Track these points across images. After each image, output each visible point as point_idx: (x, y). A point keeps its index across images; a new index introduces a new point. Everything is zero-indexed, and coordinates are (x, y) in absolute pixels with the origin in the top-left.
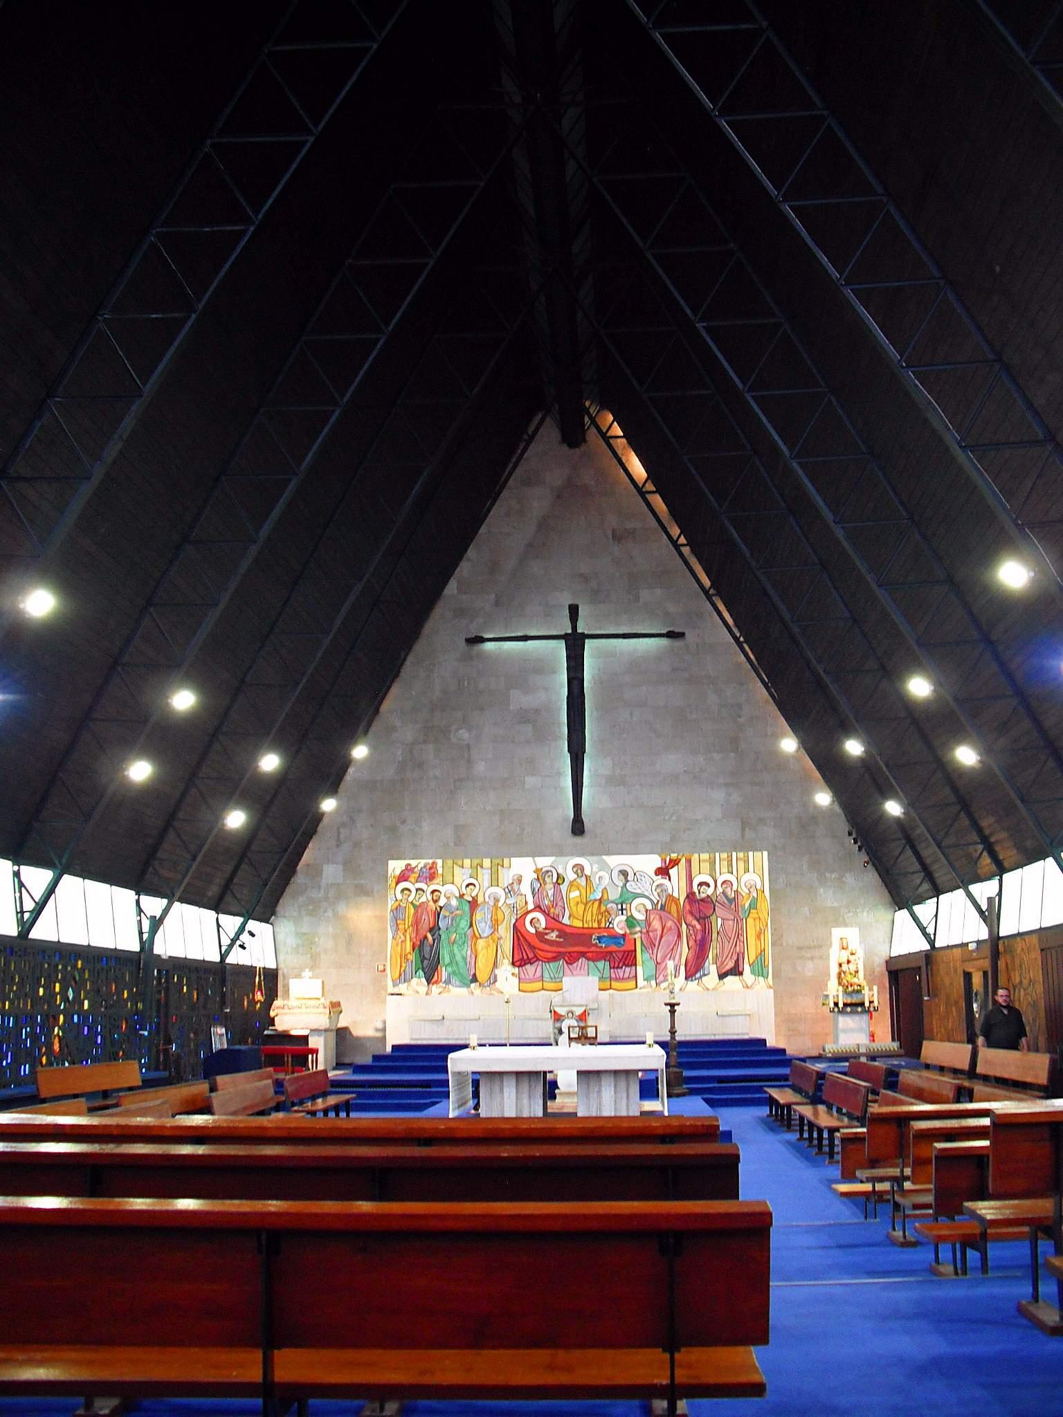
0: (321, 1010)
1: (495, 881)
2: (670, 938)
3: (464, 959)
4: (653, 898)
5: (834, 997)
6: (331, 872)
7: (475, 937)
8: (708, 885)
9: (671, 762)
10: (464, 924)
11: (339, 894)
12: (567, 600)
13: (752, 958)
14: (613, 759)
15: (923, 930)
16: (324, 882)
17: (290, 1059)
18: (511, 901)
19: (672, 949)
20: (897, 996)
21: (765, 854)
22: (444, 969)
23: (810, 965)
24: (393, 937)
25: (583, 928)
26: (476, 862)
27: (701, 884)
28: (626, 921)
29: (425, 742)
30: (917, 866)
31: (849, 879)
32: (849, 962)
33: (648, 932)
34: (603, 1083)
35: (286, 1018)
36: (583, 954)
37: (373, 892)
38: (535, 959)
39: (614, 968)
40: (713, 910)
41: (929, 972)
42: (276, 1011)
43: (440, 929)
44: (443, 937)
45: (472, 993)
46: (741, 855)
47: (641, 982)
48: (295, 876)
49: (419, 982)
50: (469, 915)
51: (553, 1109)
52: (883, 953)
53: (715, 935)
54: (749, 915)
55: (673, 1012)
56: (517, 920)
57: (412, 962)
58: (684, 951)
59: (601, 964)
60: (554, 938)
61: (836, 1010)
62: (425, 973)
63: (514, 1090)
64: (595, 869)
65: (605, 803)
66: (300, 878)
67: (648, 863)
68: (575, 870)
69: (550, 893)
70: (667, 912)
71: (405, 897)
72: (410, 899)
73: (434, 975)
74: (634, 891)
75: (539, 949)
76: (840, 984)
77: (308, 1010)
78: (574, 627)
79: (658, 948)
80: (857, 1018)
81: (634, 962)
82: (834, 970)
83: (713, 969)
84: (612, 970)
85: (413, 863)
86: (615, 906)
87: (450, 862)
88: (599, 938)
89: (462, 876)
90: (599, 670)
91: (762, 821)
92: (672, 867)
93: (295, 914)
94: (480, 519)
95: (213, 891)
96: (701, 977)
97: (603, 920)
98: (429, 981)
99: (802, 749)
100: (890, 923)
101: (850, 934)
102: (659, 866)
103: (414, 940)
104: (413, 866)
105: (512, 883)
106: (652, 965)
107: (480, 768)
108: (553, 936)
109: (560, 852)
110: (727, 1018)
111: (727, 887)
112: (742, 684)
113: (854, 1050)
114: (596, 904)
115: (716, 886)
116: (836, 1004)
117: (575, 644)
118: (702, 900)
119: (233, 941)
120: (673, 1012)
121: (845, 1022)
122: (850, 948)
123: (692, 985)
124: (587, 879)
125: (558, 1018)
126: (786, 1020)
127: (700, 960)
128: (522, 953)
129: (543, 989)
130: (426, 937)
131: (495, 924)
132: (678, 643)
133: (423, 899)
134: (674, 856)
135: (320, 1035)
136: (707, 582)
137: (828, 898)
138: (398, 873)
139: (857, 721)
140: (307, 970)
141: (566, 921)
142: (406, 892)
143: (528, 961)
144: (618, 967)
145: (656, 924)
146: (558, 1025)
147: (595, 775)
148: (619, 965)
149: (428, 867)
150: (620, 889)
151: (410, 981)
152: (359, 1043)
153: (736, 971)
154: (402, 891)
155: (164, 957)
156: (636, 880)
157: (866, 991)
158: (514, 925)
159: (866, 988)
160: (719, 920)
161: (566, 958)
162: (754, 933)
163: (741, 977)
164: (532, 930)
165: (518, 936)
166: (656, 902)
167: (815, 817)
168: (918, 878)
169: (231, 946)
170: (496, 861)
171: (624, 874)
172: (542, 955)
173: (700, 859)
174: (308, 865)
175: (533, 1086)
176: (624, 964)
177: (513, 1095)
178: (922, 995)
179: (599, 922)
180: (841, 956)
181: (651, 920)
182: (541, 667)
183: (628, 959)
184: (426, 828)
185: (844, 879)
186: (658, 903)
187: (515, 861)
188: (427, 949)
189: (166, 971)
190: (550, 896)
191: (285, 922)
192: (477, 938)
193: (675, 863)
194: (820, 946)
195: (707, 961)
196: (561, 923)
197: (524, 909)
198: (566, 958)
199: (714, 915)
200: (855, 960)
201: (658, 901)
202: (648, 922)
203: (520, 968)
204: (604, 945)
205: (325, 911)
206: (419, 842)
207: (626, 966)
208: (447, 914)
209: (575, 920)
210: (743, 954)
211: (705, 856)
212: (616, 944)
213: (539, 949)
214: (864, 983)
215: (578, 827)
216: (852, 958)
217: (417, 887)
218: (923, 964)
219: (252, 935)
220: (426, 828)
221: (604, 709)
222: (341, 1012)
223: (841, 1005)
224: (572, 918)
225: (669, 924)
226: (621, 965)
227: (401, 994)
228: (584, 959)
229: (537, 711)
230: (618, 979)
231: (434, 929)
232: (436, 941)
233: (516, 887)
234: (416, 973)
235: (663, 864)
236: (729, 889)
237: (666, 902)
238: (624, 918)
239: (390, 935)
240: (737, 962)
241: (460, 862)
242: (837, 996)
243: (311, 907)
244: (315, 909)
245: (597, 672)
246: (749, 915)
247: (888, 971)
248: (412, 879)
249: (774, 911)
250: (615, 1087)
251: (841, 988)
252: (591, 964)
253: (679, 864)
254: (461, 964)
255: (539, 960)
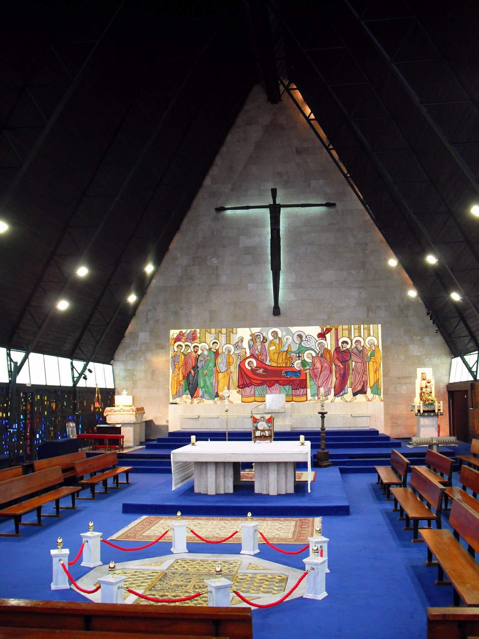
0: (131, 412)
1: (228, 341)
2: (326, 372)
3: (212, 384)
4: (316, 350)
5: (418, 407)
6: (143, 336)
7: (218, 372)
8: (347, 343)
9: (329, 275)
10: (211, 364)
11: (148, 348)
12: (270, 186)
13: (372, 384)
14: (296, 274)
15: (470, 369)
16: (139, 343)
17: (107, 441)
18: (237, 352)
19: (327, 379)
20: (453, 402)
21: (380, 326)
22: (200, 389)
23: (404, 387)
24: (173, 372)
25: (277, 367)
26: (218, 330)
27: (344, 342)
28: (301, 363)
29: (193, 265)
30: (467, 333)
31: (427, 340)
32: (426, 387)
33: (313, 369)
34: (270, 469)
35: (113, 417)
36: (277, 382)
37: (165, 347)
38: (250, 384)
39: (294, 389)
40: (350, 357)
41: (473, 394)
42: (107, 413)
43: (198, 367)
44: (200, 372)
45: (216, 402)
46: (366, 326)
47: (309, 397)
48: (124, 339)
49: (187, 397)
50: (214, 359)
51: (247, 477)
52: (445, 381)
53: (351, 371)
54: (370, 360)
55: (323, 417)
56: (240, 362)
57: (183, 385)
58: (334, 379)
59: (287, 387)
60: (261, 373)
61: (419, 414)
62: (190, 392)
63: (214, 473)
64: (284, 334)
65: (292, 297)
66: (126, 340)
67: (314, 331)
68: (273, 334)
69: (259, 347)
70: (324, 358)
71: (179, 350)
72: (182, 351)
73: (195, 393)
74: (306, 346)
75: (252, 379)
76: (421, 399)
77: (124, 412)
78: (274, 201)
79: (319, 378)
80: (431, 419)
81: (306, 386)
82: (418, 391)
83: (350, 390)
84: (293, 390)
85: (184, 331)
86: (295, 355)
87: (203, 330)
88: (286, 373)
89: (210, 338)
90: (288, 224)
91: (378, 307)
92: (327, 333)
93: (124, 359)
94: (221, 142)
95: (68, 346)
96: (343, 395)
97: (288, 362)
98: (192, 396)
99: (400, 265)
100: (449, 364)
101: (428, 372)
102: (320, 332)
103: (184, 374)
104: (184, 332)
105: (238, 342)
106: (315, 387)
107: (223, 279)
108: (261, 371)
109: (266, 324)
110: (357, 418)
111: (358, 344)
112: (368, 232)
113: (430, 441)
114: (285, 353)
115: (352, 344)
116: (419, 411)
117: (275, 210)
118: (344, 351)
119: (80, 375)
120: (323, 417)
121: (424, 421)
122: (427, 379)
123: (338, 399)
124: (279, 339)
125: (255, 421)
126: (391, 418)
127: (343, 385)
128: (243, 381)
129: (255, 401)
130: (190, 372)
131: (229, 364)
132: (332, 210)
133: (189, 351)
134: (328, 327)
135: (131, 426)
136: (346, 172)
137: (415, 350)
138: (175, 336)
139: (434, 244)
140: (125, 390)
141: (268, 363)
142: (180, 347)
143: (246, 385)
144: (296, 389)
145: (318, 365)
146: (255, 425)
147: (286, 283)
148: (297, 388)
149: (192, 333)
150: (298, 345)
151: (182, 396)
152: (159, 428)
153: (363, 391)
154: (178, 346)
155: (28, 385)
156: (307, 340)
157: (436, 404)
158: (239, 365)
159: (436, 402)
160: (354, 363)
161: (268, 383)
162: (373, 370)
163: (365, 395)
164: (249, 368)
165: (241, 371)
166: (318, 352)
167: (409, 304)
168: (467, 340)
169: (79, 378)
170: (229, 330)
171: (300, 336)
172: (254, 382)
173: (343, 329)
174: (131, 333)
175: (227, 470)
176: (300, 387)
177: (214, 476)
178: (468, 407)
179: (286, 364)
180: (422, 383)
181: (315, 363)
182: (256, 223)
183: (303, 385)
184: (194, 312)
185: (424, 340)
186: (319, 353)
187: (239, 330)
188: (191, 378)
189: (32, 393)
190: (259, 349)
191: (119, 364)
192: (219, 372)
193: (328, 331)
194: (411, 377)
195: (347, 385)
196: (265, 364)
197: (244, 356)
198: (268, 383)
199: (351, 359)
200: (430, 386)
201: (319, 352)
202: (313, 364)
203: (242, 389)
204: (289, 377)
205: (140, 358)
206: (190, 320)
207: (301, 389)
208: (202, 359)
209: (273, 362)
210: (367, 381)
211: (346, 327)
212: (295, 376)
213: (252, 379)
214: (435, 399)
215: (276, 311)
216: (428, 385)
217: (185, 344)
218: (469, 388)
219: (90, 371)
220: (194, 312)
221: (291, 246)
222: (144, 413)
223: (422, 411)
224: (271, 361)
225: (325, 365)
226: (298, 388)
227: (176, 404)
228: (278, 384)
229: (255, 248)
230: (296, 395)
231: (195, 367)
232: (196, 374)
233: (240, 344)
234: (185, 392)
235: (322, 331)
236: (359, 345)
237: (323, 353)
238: (300, 361)
239: (171, 371)
240: (363, 386)
241: (209, 330)
242: (420, 406)
243: (132, 356)
244: (134, 356)
245: (288, 226)
246: (370, 360)
247: (448, 391)
248: (183, 340)
249: (385, 357)
250: (278, 471)
251: (422, 402)
252: (282, 387)
253: (331, 332)
254: (210, 387)
255: (253, 385)
